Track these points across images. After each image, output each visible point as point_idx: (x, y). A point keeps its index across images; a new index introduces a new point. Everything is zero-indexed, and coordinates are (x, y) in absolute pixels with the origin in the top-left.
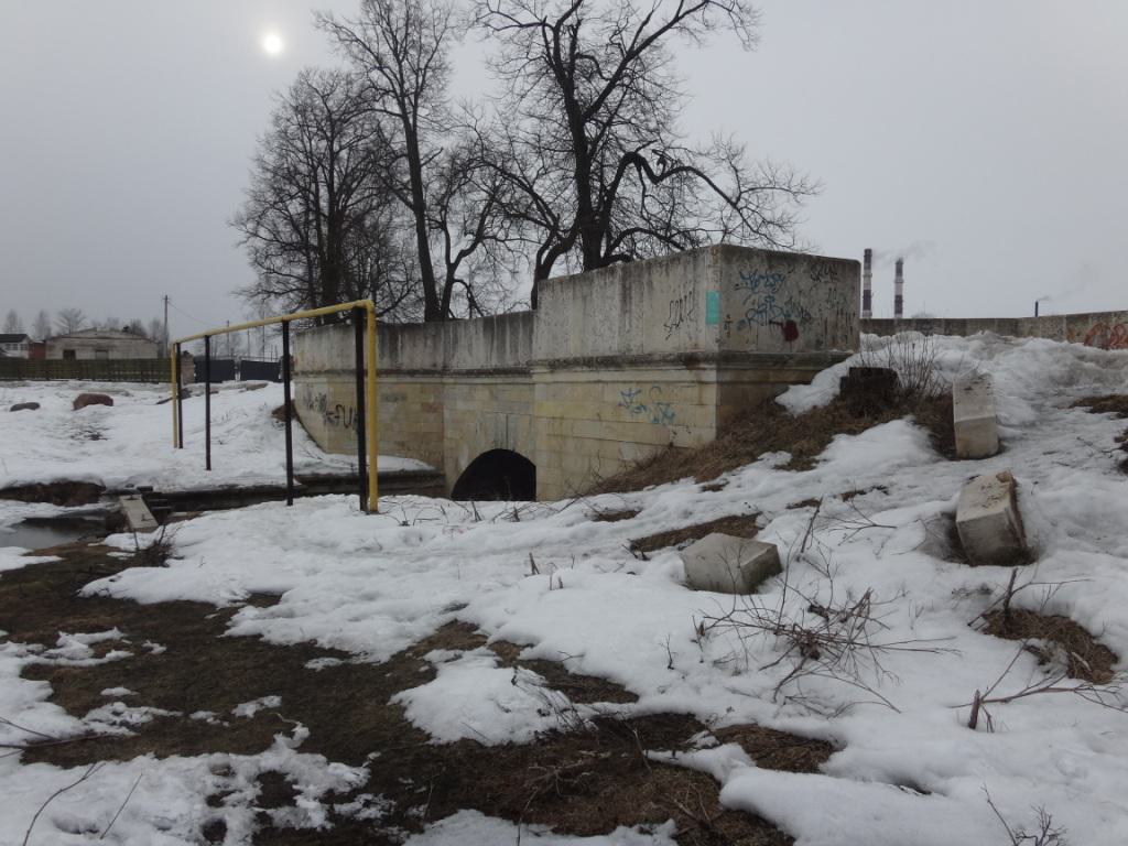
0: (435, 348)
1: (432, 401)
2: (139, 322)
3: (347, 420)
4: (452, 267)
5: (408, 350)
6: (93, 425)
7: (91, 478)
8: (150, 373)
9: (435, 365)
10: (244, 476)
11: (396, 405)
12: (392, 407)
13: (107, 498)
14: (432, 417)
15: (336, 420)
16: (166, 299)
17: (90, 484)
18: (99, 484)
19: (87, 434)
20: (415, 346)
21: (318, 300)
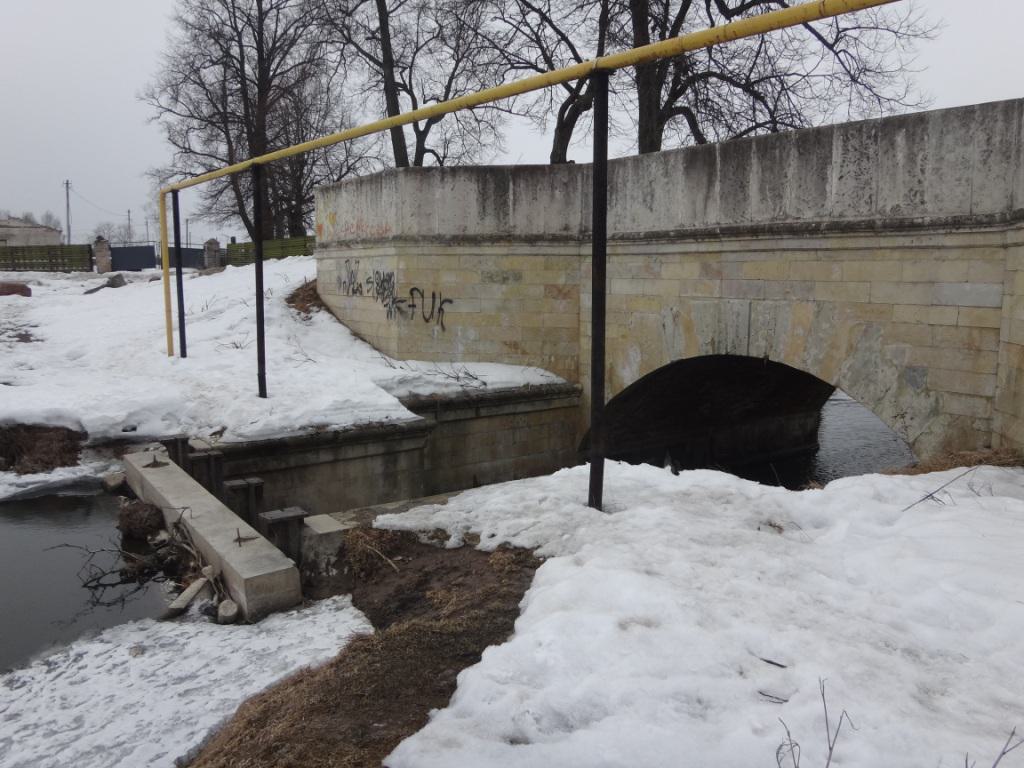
0: (568, 203)
1: (561, 281)
2: (31, 215)
3: (428, 311)
4: (421, 136)
5: (524, 207)
6: (13, 320)
7: (59, 417)
8: (60, 261)
9: (566, 228)
10: (338, 408)
11: (504, 287)
12: (498, 291)
13: (91, 452)
14: (561, 305)
15: (410, 311)
16: (67, 184)
17: (57, 429)
18: (74, 428)
19: (11, 333)
20: (535, 199)
21: (667, 34)
